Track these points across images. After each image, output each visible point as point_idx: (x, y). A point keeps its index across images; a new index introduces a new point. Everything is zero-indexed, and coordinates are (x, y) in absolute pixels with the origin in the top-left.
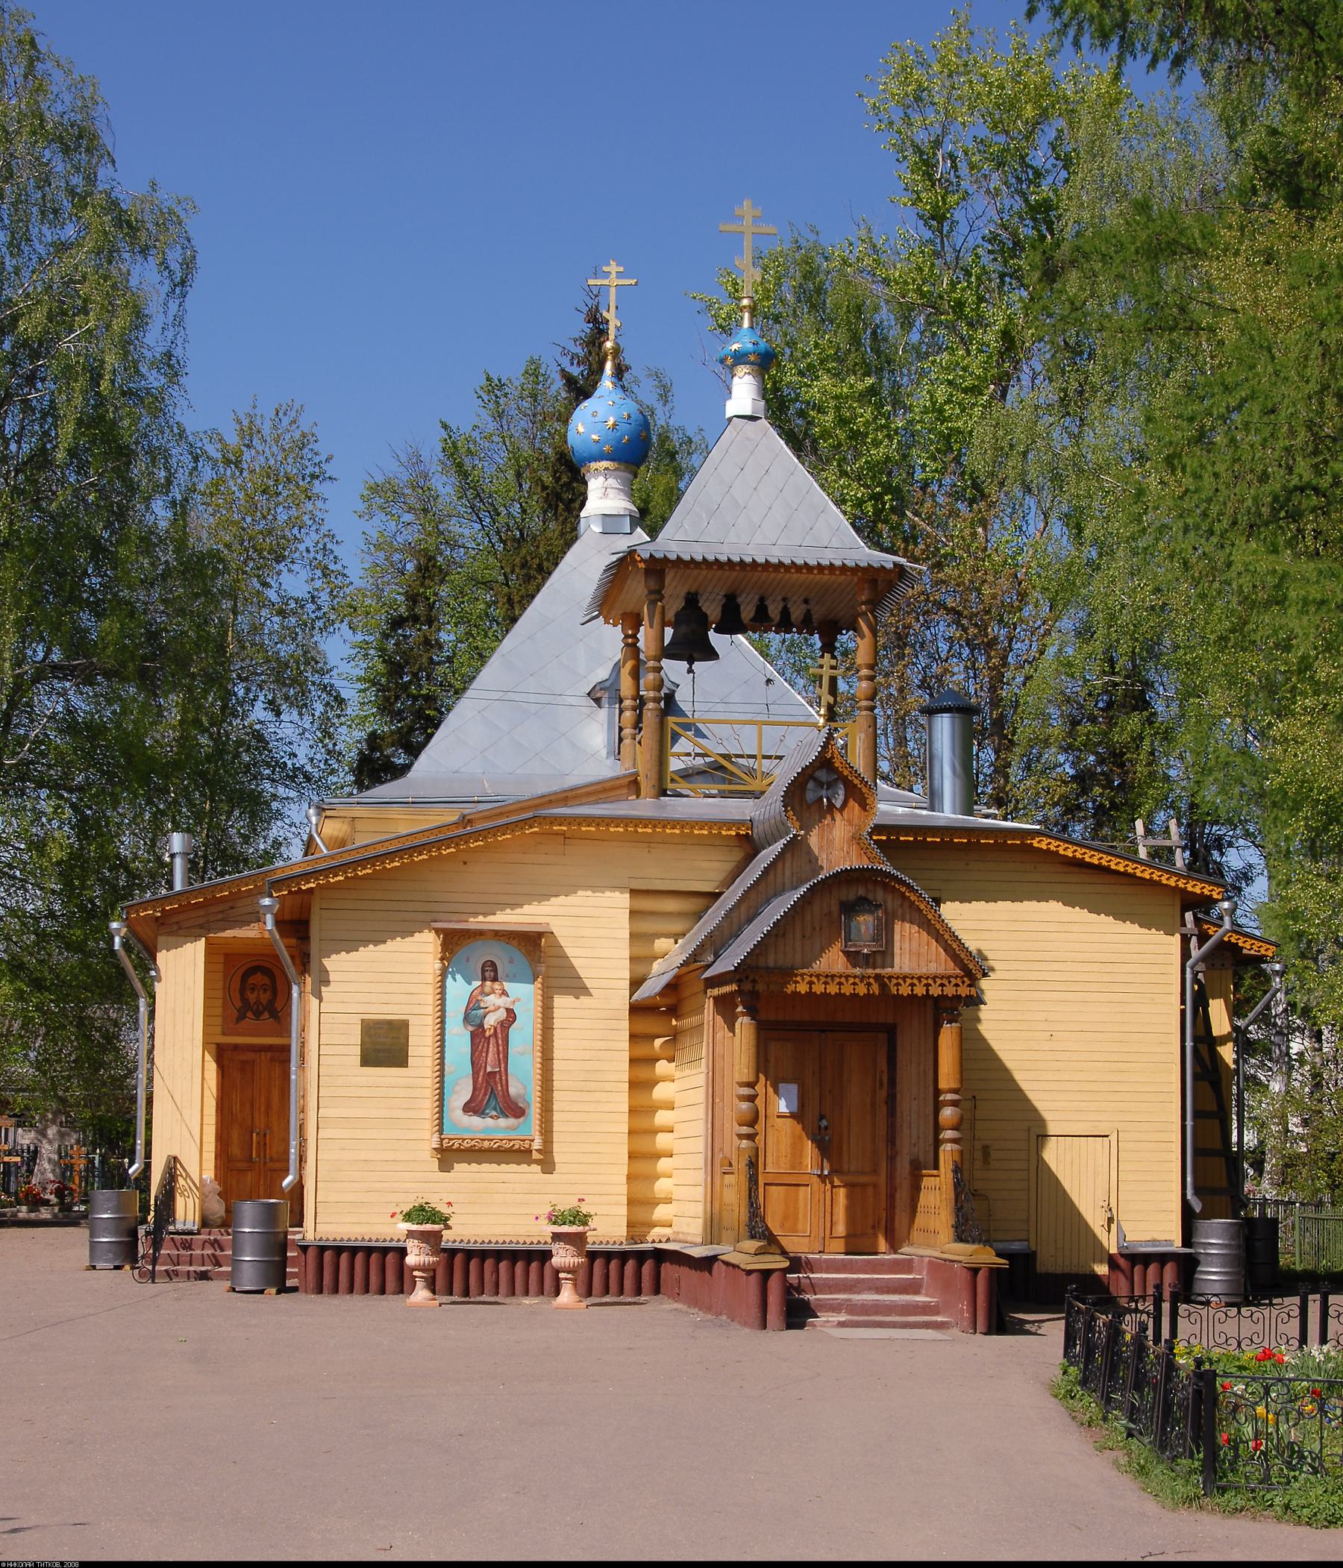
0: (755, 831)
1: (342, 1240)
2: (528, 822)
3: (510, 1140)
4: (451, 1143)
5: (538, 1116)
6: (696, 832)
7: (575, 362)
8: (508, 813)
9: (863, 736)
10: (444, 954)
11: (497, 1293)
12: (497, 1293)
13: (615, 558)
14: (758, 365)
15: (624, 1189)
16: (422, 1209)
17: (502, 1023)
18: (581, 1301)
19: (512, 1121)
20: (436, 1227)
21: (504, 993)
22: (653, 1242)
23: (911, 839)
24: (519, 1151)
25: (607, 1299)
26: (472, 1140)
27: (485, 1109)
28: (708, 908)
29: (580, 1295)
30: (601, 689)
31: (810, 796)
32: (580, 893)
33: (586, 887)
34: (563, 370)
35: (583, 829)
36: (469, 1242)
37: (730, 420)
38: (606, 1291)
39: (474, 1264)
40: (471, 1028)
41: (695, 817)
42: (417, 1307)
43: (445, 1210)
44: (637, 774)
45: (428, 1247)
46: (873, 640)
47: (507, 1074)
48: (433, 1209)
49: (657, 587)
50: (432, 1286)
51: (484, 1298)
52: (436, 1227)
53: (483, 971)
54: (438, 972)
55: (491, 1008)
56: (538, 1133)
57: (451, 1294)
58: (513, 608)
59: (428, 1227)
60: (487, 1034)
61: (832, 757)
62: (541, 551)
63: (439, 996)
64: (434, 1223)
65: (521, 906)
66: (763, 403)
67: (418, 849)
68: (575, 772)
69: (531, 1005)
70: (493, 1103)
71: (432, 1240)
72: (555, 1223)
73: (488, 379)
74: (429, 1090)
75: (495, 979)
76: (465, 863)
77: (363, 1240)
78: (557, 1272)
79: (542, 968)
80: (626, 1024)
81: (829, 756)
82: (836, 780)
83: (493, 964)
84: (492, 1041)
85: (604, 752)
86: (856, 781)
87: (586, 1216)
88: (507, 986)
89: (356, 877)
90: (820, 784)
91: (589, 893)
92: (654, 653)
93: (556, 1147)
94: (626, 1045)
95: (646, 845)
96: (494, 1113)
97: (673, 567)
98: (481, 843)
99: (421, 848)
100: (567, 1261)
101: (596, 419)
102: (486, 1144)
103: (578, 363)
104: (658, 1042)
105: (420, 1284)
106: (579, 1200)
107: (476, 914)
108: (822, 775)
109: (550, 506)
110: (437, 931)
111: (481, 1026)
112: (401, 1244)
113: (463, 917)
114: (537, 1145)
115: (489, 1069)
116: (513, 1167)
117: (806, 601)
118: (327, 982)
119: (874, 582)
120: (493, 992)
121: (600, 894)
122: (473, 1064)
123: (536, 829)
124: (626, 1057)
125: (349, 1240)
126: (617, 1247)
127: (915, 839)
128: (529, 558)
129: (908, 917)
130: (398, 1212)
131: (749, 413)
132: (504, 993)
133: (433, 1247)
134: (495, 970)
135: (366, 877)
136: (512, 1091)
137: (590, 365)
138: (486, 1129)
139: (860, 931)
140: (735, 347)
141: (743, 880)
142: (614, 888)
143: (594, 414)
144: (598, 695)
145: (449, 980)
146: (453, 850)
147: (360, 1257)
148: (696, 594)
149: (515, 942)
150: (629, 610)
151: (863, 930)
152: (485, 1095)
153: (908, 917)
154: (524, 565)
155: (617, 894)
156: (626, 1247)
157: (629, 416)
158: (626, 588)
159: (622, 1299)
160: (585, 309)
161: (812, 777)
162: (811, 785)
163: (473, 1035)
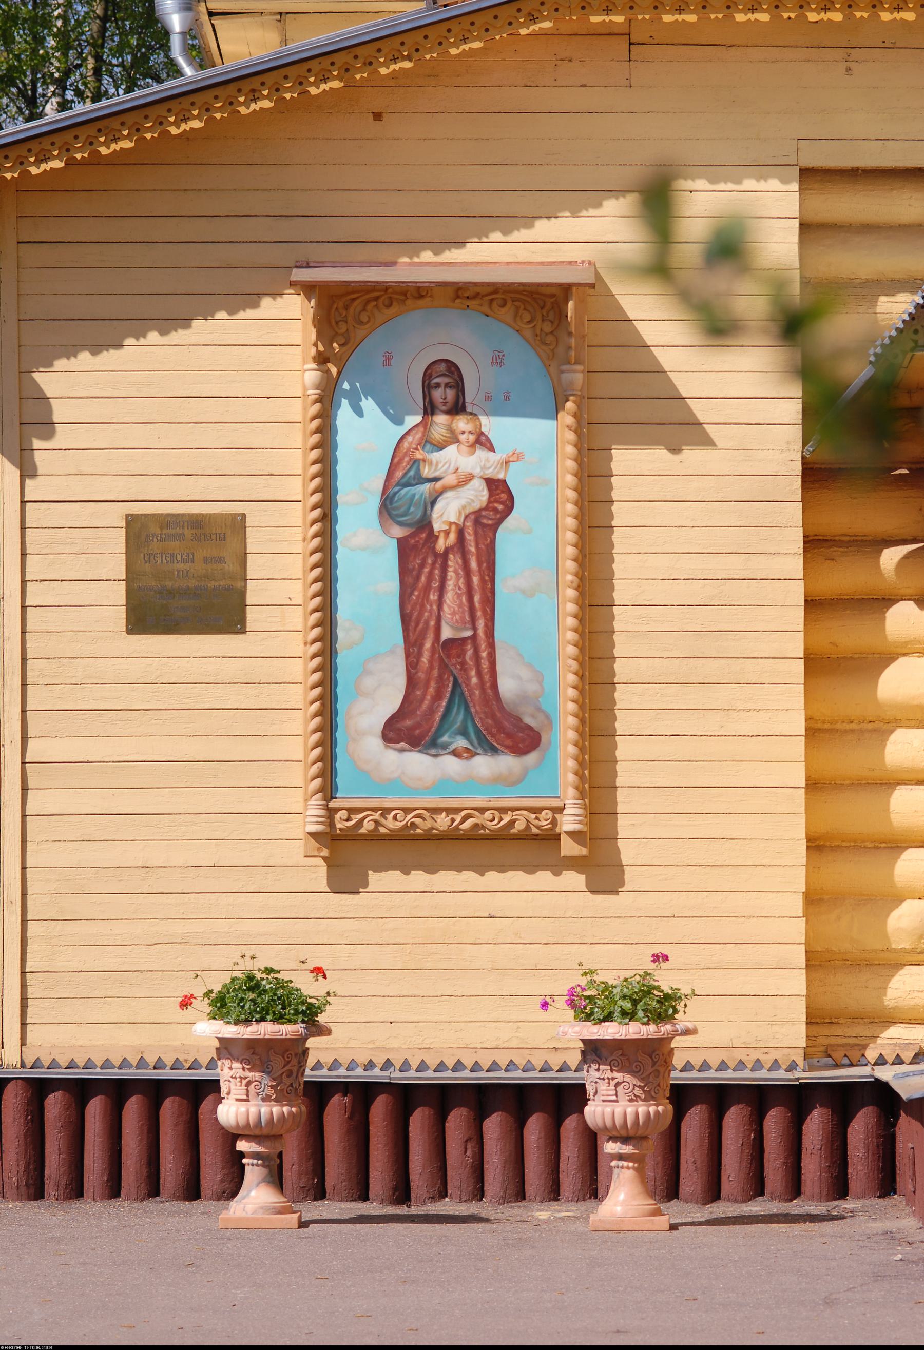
1: (54, 1065)
3: (503, 810)
4: (356, 818)
5: (572, 749)
8: (292, 50)
10: (328, 344)
11: (479, 1193)
12: (479, 1193)
15: (797, 929)
16: (252, 984)
17: (477, 517)
18: (657, 1213)
19: (506, 762)
20: (286, 1030)
21: (482, 441)
22: (881, 1061)
24: (526, 837)
25: (756, 1207)
26: (407, 811)
27: (439, 733)
29: (652, 1194)
35: (667, 18)
36: (405, 1066)
38: (757, 1188)
39: (419, 1120)
40: (399, 532)
42: (616, 1231)
43: (309, 988)
45: (267, 1081)
47: (492, 645)
48: (282, 985)
50: (277, 1179)
51: (446, 1207)
52: (286, 1030)
53: (428, 386)
54: (313, 393)
55: (450, 479)
56: (571, 792)
57: (364, 1196)
59: (266, 1030)
60: (441, 545)
63: (315, 454)
64: (279, 1019)
65: (528, 220)
67: (247, 86)
69: (550, 472)
70: (458, 717)
71: (277, 1063)
72: (588, 1017)
74: (299, 689)
75: (457, 408)
76: (378, 116)
77: (142, 1064)
78: (231, 1137)
79: (576, 377)
80: (794, 512)
83: (453, 369)
84: (454, 562)
87: (667, 997)
88: (491, 425)
89: (96, 160)
93: (624, 827)
94: (796, 565)
95: (841, 53)
96: (461, 743)
98: (407, 65)
99: (255, 82)
100: (619, 1110)
102: (442, 822)
104: (891, 557)
105: (253, 1172)
106: (656, 958)
107: (414, 244)
110: (308, 289)
111: (425, 524)
112: (202, 1074)
113: (384, 253)
114: (569, 822)
115: (447, 633)
116: (516, 878)
118: (47, 427)
120: (453, 439)
122: (405, 619)
123: (547, 25)
124: (797, 593)
125: (107, 1064)
126: (781, 1076)
130: (199, 992)
132: (482, 441)
133: (278, 1079)
134: (458, 385)
135: (119, 160)
136: (507, 686)
138: (442, 783)
145: (344, 414)
146: (336, 84)
147: (133, 1108)
149: (507, 312)
152: (438, 697)
156: (802, 1075)
159: (797, 1207)
163: (405, 549)
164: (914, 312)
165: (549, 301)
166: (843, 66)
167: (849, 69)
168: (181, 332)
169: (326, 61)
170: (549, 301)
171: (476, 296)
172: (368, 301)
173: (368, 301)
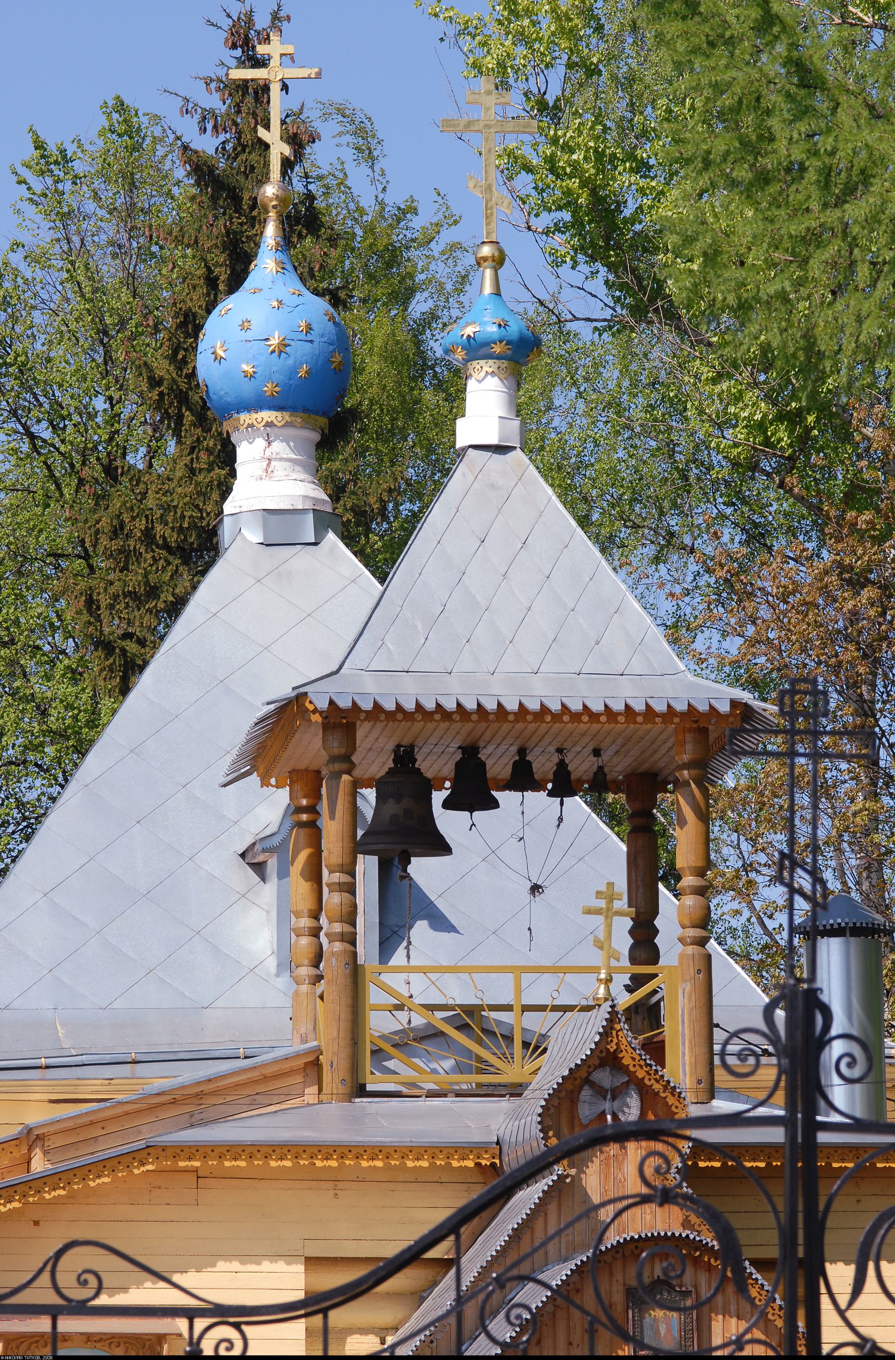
0: (506, 1159)
2: (138, 1156)
6: (410, 1164)
7: (209, 126)
9: (688, 987)
13: (272, 707)
14: (509, 359)
23: (762, 1165)
28: (435, 1284)
30: (264, 851)
31: (586, 1111)
32: (221, 1265)
33: (228, 1257)
34: (185, 148)
37: (465, 449)
41: (406, 1140)
44: (318, 1051)
46: (701, 826)
49: (343, 751)
58: (98, 619)
61: (618, 1050)
62: (150, 502)
66: (516, 423)
68: (220, 1003)
73: (39, 145)
76: (36, 1223)
81: (612, 1047)
82: (627, 1083)
85: (271, 964)
86: (657, 1087)
90: (601, 1092)
91: (235, 1265)
92: (340, 861)
95: (331, 1185)
97: (366, 719)
101: (250, 335)
103: (215, 127)
108: (604, 1077)
109: (166, 415)
117: (597, 752)
119: (703, 732)
121: (253, 1267)
127: (769, 1164)
128: (126, 517)
129: (733, 1308)
131: (494, 440)
137: (239, 133)
139: (657, 1332)
140: (469, 331)
141: (486, 1241)
142: (275, 1257)
143: (245, 326)
144: (260, 858)
148: (412, 747)
150: (302, 765)
151: (663, 1331)
153: (733, 1308)
154: (117, 531)
155: (281, 1266)
157: (309, 328)
158: (294, 742)
160: (227, 23)
161: (587, 1081)
162: (586, 1093)
164: (629, 983)
165: (148, 1343)
166: (332, 1192)
167: (336, 1195)
168: (122, 1295)
169: (11, 1190)
170: (148, 1343)
171: (101, 1340)
172: (31, 1344)
173: (31, 1344)
